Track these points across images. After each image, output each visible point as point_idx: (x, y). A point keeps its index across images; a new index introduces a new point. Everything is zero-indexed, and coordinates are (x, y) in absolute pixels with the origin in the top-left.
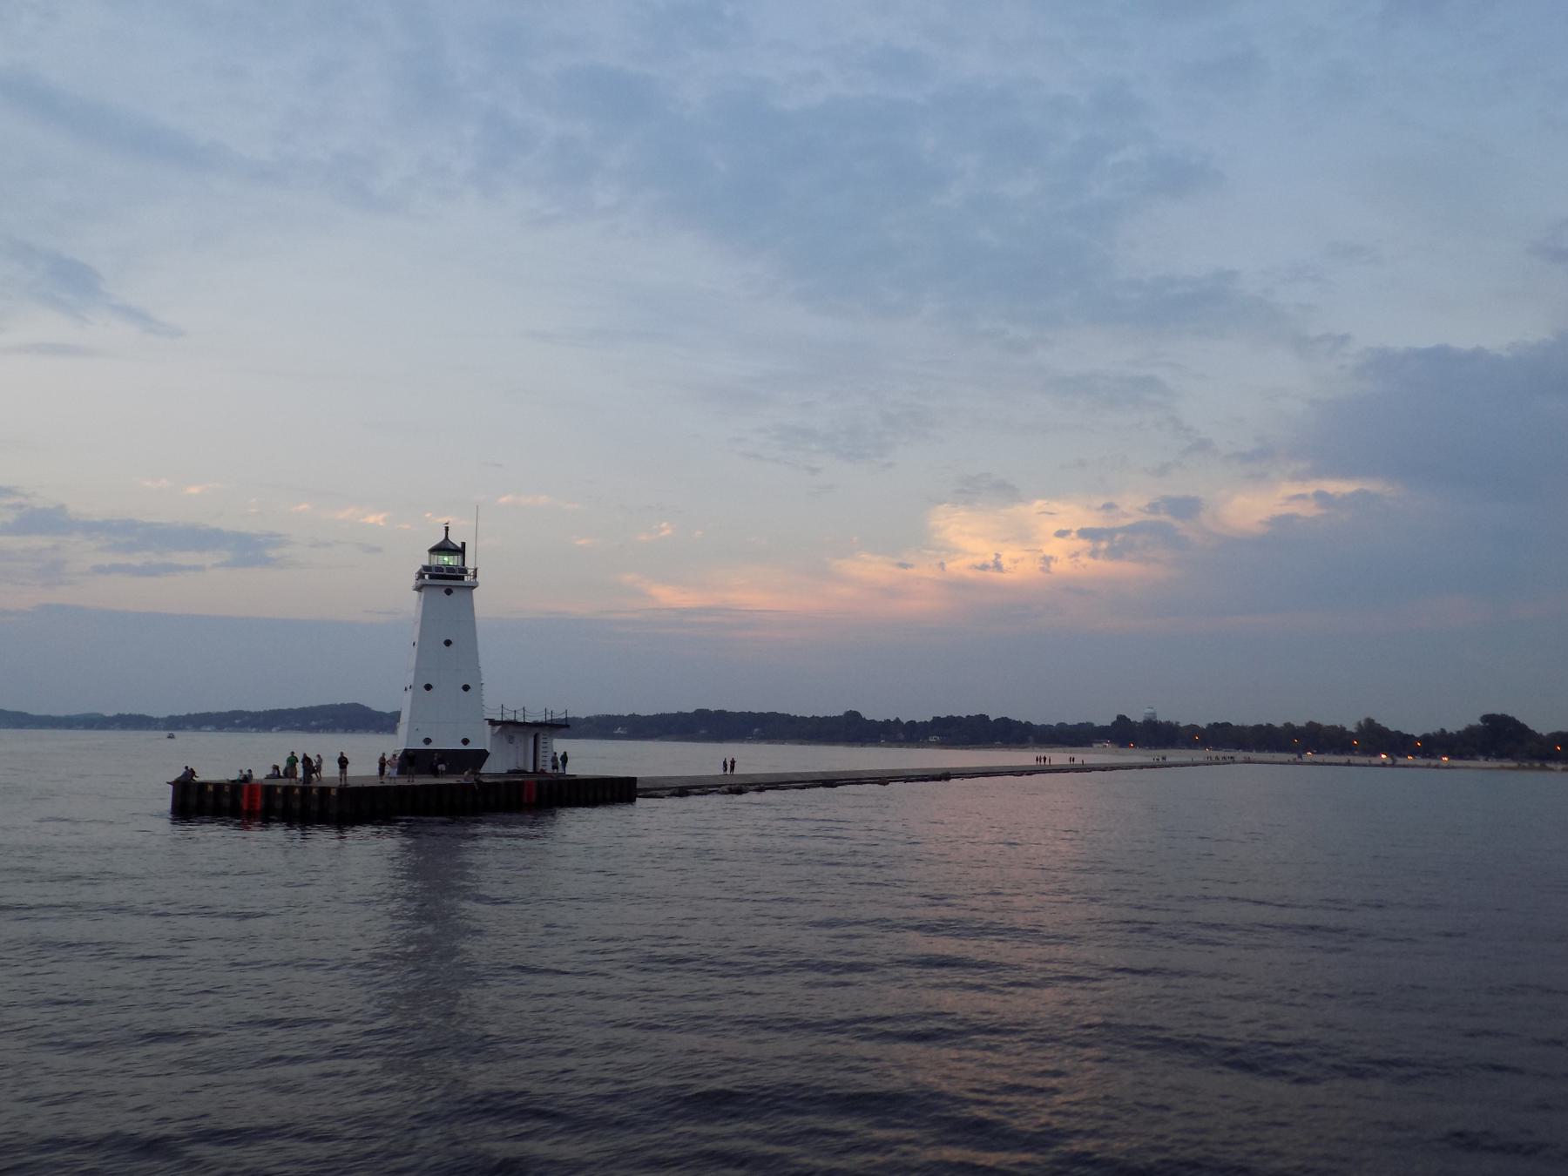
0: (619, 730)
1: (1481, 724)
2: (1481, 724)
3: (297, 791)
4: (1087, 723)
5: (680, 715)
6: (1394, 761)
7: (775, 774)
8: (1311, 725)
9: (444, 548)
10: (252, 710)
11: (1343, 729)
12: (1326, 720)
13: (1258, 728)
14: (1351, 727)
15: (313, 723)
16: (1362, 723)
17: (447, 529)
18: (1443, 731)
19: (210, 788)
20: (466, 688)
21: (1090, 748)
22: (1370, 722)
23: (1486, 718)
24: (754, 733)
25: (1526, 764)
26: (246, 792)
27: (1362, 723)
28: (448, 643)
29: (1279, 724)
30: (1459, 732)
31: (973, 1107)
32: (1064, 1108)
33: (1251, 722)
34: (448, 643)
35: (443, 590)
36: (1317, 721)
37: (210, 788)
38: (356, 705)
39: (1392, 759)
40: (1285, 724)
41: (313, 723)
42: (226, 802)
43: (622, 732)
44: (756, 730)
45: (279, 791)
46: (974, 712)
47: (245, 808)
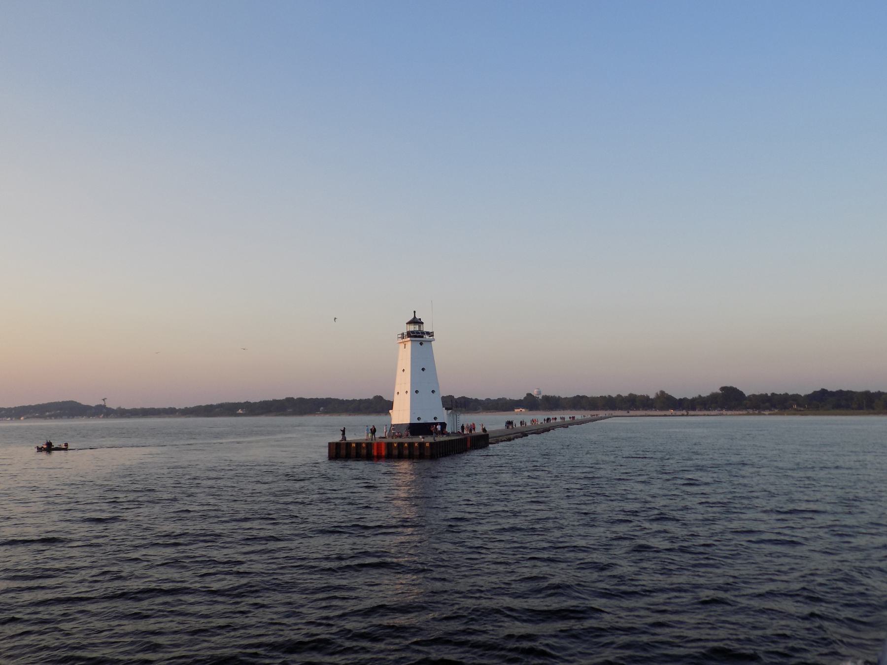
0: (240, 411)
1: (721, 392)
2: (721, 392)
3: (406, 445)
4: (503, 398)
5: (275, 401)
6: (688, 413)
7: (497, 430)
8: (631, 395)
9: (415, 321)
10: (6, 407)
11: (648, 397)
12: (639, 392)
13: (603, 398)
14: (652, 396)
15: (47, 413)
16: (659, 393)
17: (415, 312)
18: (700, 396)
19: (354, 445)
20: (433, 392)
21: (512, 412)
22: (662, 393)
23: (723, 389)
24: (321, 410)
25: (757, 412)
26: (375, 447)
27: (659, 393)
28: (423, 369)
29: (614, 395)
30: (707, 396)
31: (885, 581)
32: (683, 594)
33: (597, 394)
34: (423, 369)
35: (419, 342)
36: (634, 393)
37: (354, 445)
38: (72, 402)
39: (687, 412)
40: (618, 395)
41: (47, 413)
42: (364, 452)
43: (241, 412)
44: (322, 408)
45: (395, 445)
46: (795, 393)
47: (375, 454)
